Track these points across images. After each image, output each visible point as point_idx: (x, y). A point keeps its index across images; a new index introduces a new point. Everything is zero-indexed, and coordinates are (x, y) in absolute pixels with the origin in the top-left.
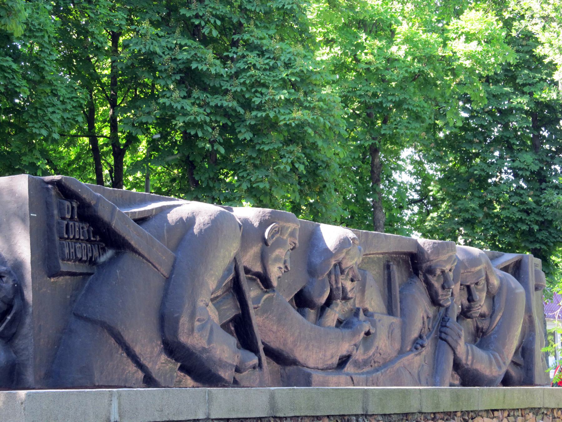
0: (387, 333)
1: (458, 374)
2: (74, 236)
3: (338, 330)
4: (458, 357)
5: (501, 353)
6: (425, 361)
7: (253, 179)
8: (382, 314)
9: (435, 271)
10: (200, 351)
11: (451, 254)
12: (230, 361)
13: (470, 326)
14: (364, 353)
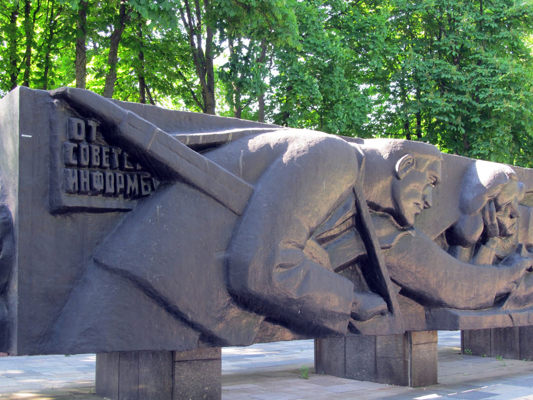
2: (90, 162)
3: (495, 268)
10: (285, 303)
12: (341, 310)
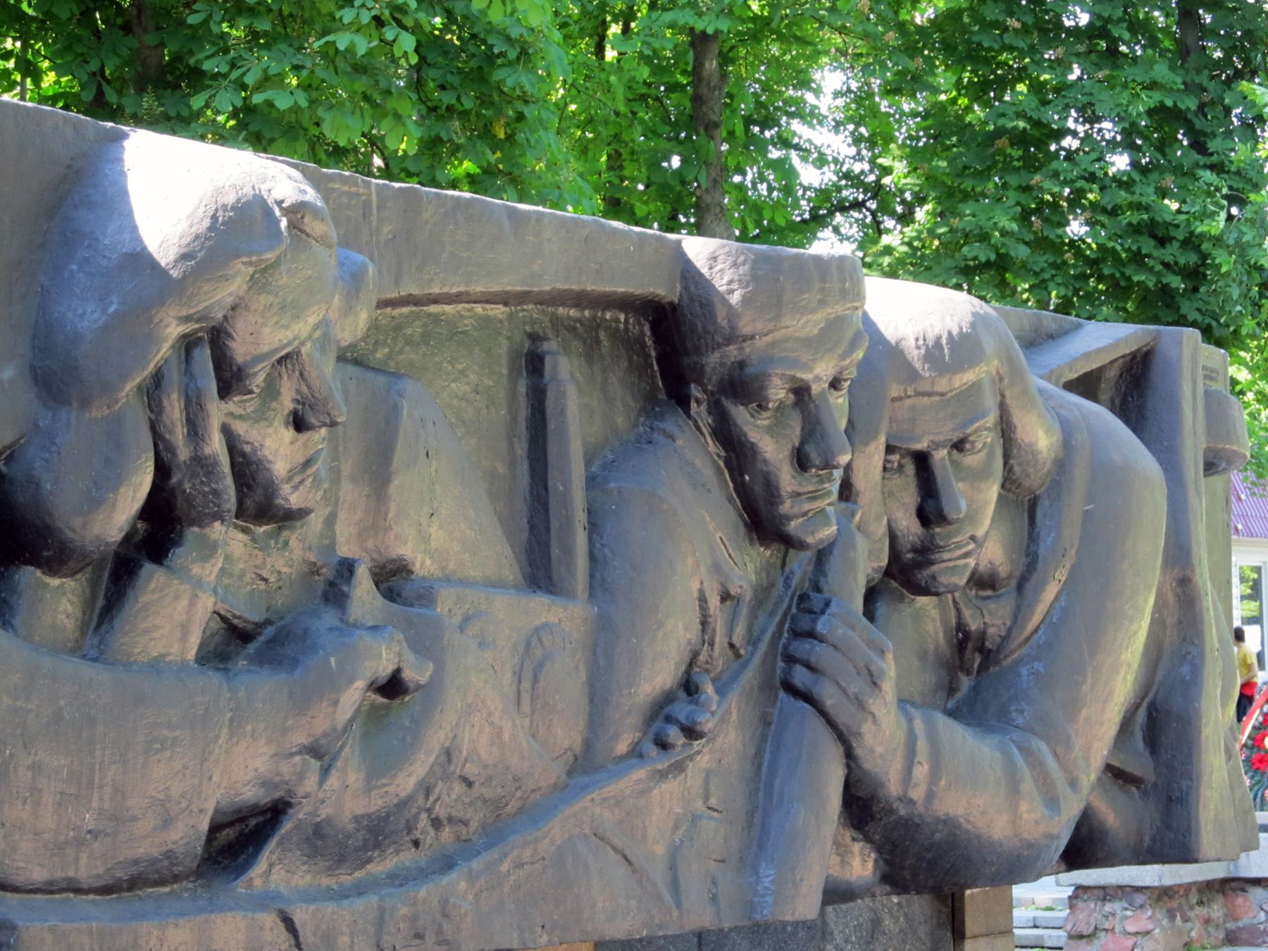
0: (507, 678)
1: (868, 839)
3: (213, 679)
4: (866, 773)
5: (1060, 743)
6: (706, 798)
7: (249, 80)
8: (496, 584)
9: (763, 388)
11: (838, 309)
13: (930, 628)
14: (369, 789)
